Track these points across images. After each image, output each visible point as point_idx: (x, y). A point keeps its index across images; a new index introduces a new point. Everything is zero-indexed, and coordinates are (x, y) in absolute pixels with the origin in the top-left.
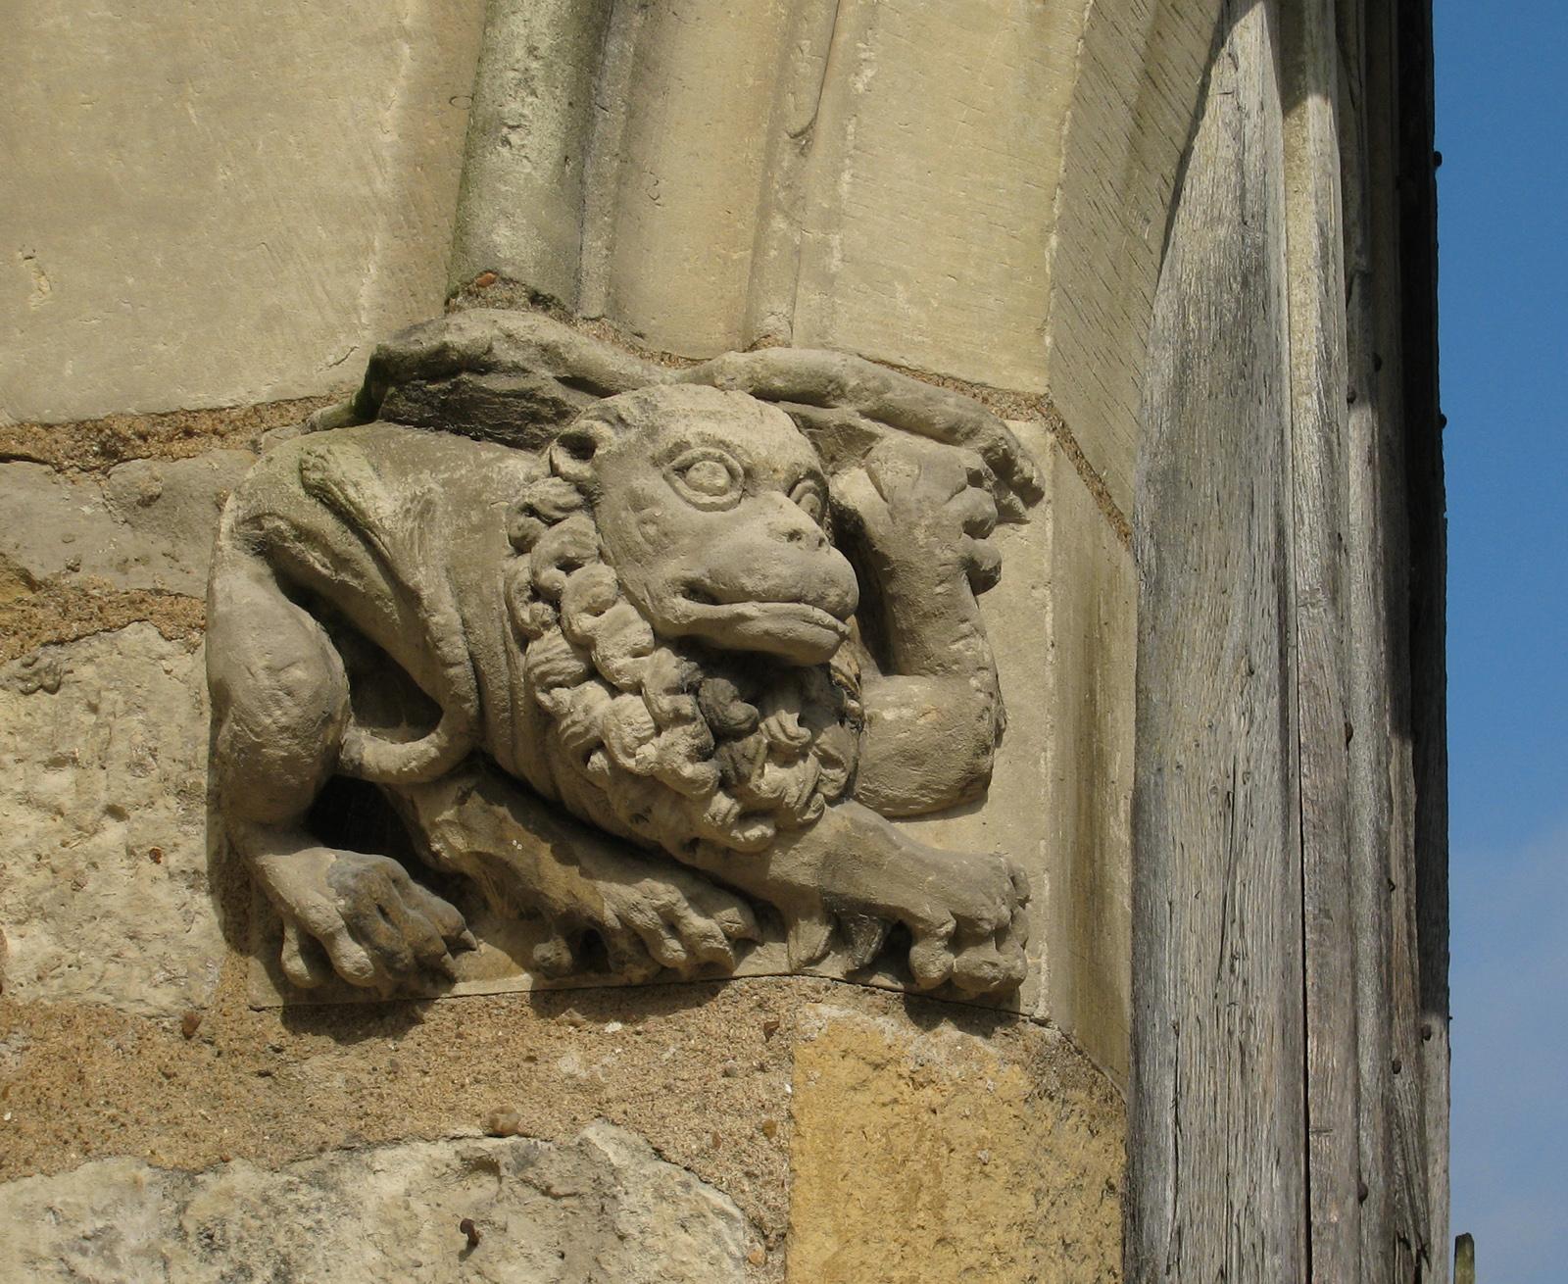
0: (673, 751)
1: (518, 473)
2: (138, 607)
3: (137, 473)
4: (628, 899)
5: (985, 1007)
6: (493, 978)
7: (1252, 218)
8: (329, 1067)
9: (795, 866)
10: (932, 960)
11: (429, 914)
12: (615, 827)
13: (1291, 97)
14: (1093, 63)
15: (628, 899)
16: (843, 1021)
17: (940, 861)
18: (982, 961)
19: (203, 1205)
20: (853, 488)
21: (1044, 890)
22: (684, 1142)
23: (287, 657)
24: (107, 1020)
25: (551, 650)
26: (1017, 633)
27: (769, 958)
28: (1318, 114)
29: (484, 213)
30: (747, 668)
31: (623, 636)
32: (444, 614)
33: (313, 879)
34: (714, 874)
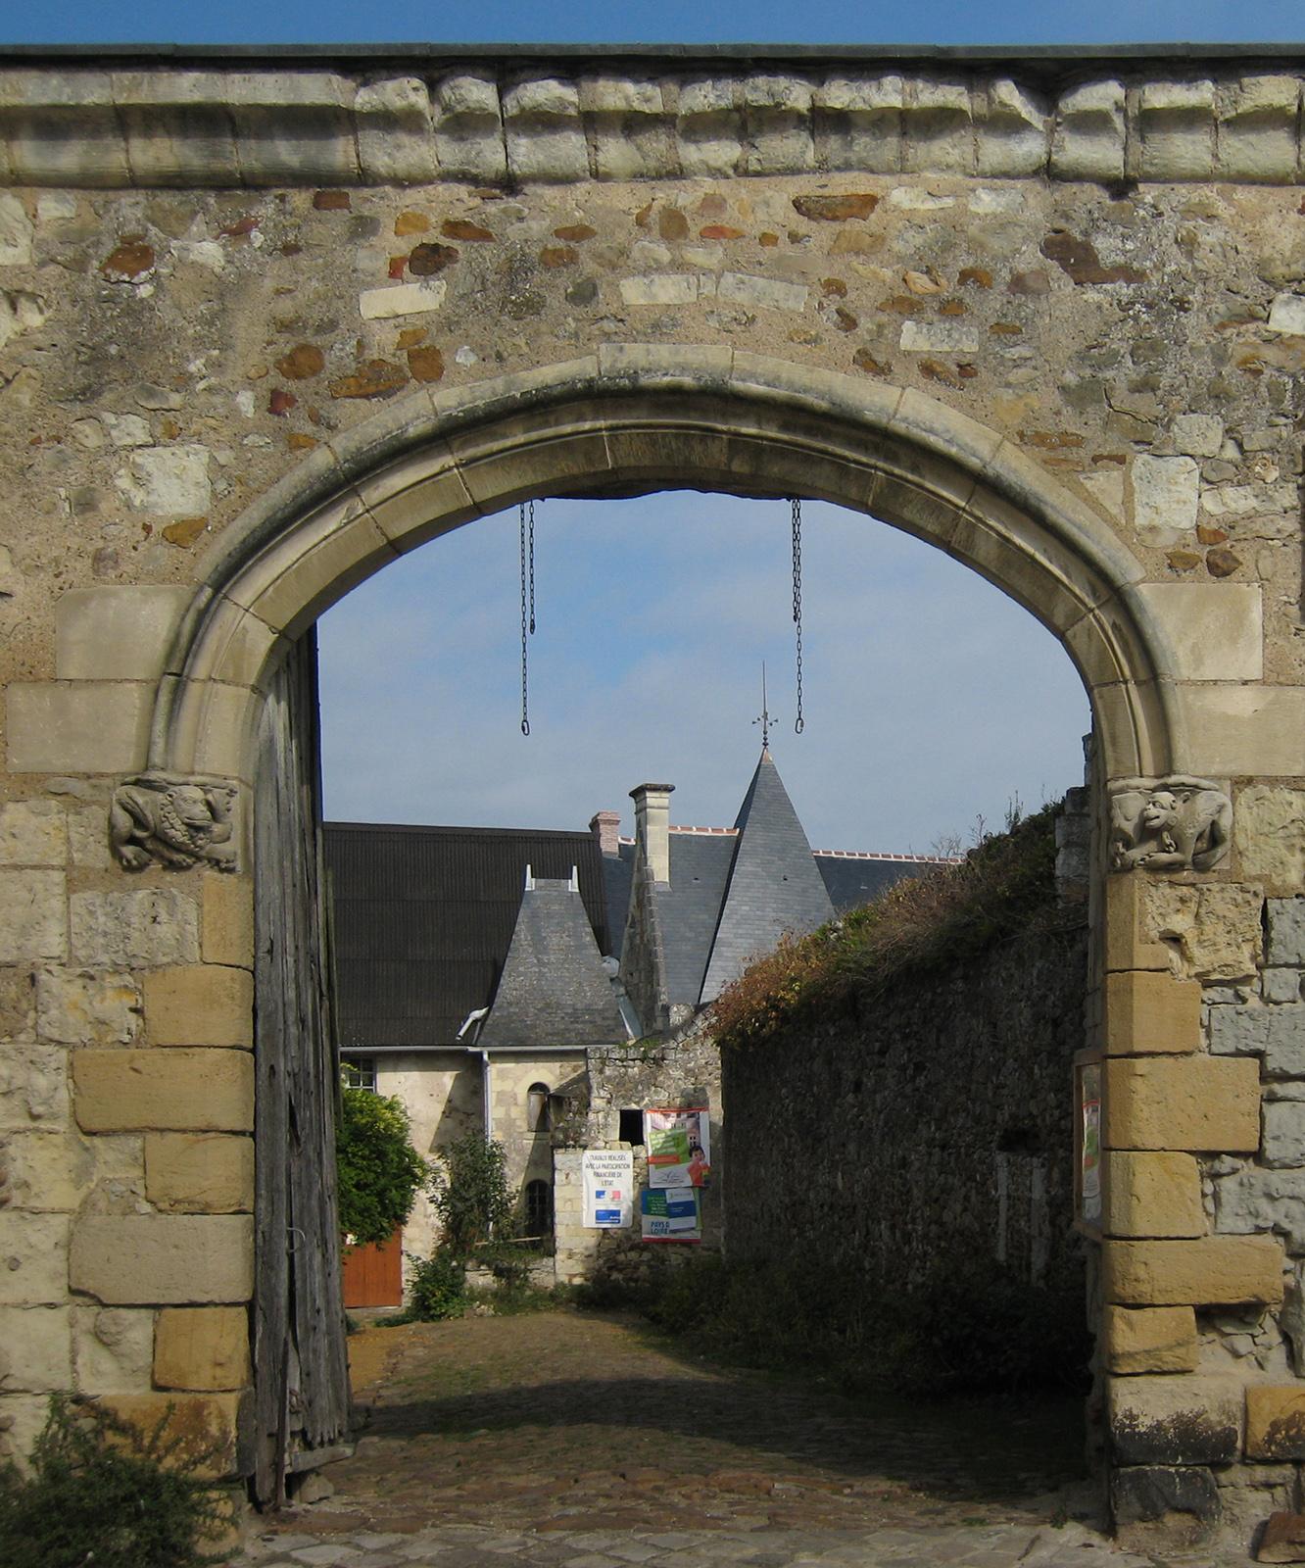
0: (186, 840)
1: (160, 796)
2: (94, 803)
3: (94, 781)
4: (177, 857)
5: (231, 871)
6: (156, 865)
7: (271, 729)
8: (129, 878)
9: (203, 853)
10: (223, 865)
11: (146, 856)
12: (178, 848)
13: (278, 702)
14: (245, 723)
15: (177, 857)
16: (209, 873)
17: (225, 849)
18: (231, 865)
19: (110, 897)
20: (210, 797)
21: (239, 851)
22: (186, 891)
23: (124, 821)
24: (93, 869)
25: (167, 824)
26: (234, 819)
27: (198, 865)
28: (283, 705)
29: (152, 754)
30: (194, 828)
31: (178, 824)
32: (150, 818)
33: (129, 851)
34: (191, 854)
